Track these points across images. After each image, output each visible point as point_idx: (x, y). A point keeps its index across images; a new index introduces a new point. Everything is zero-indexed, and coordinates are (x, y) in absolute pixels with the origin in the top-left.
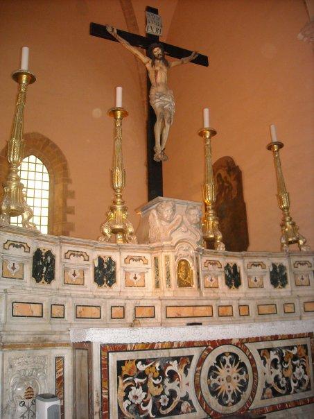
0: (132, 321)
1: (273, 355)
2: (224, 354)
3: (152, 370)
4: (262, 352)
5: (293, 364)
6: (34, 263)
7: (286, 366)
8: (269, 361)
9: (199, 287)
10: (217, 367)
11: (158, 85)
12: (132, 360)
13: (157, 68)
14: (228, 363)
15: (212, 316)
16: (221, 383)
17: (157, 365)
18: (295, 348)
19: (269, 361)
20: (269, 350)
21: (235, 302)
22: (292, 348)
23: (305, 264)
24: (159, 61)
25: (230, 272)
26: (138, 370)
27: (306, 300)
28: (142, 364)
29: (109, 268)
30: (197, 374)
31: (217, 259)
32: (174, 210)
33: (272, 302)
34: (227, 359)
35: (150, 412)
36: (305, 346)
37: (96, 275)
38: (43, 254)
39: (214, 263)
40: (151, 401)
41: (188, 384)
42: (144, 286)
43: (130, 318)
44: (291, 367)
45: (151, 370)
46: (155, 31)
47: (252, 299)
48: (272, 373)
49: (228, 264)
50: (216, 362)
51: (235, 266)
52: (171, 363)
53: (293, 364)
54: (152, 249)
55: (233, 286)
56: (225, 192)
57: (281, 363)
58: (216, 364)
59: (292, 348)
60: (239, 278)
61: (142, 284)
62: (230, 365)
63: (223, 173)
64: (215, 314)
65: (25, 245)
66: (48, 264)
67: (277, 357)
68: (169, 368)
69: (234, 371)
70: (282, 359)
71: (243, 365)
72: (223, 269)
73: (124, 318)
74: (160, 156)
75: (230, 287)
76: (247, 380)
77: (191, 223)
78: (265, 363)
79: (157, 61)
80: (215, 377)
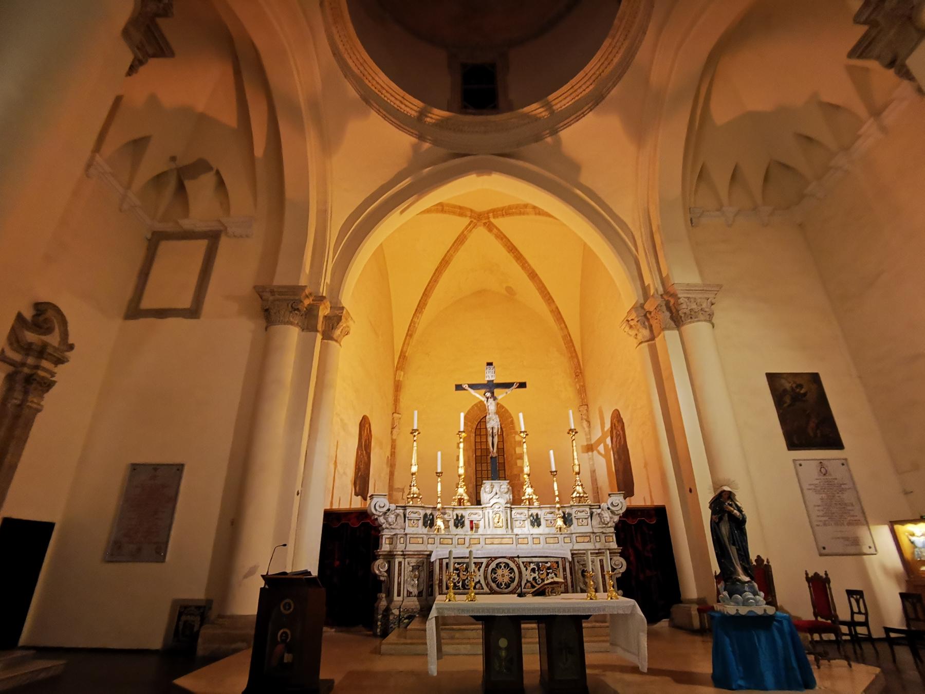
1: (532, 566)
2: (500, 563)
4: (525, 564)
5: (547, 572)
7: (542, 572)
8: (529, 569)
14: (503, 567)
16: (498, 577)
17: (465, 565)
19: (529, 569)
20: (530, 563)
22: (547, 563)
23: (416, 513)
27: (577, 535)
29: (461, 519)
30: (485, 571)
31: (523, 511)
33: (555, 536)
34: (503, 565)
35: (461, 586)
36: (557, 563)
37: (455, 523)
40: (461, 582)
41: (480, 576)
43: (467, 544)
44: (545, 574)
48: (531, 575)
51: (537, 515)
53: (547, 572)
55: (536, 526)
57: (538, 570)
59: (547, 563)
60: (540, 522)
63: (53, 339)
67: (535, 567)
69: (506, 572)
70: (539, 568)
71: (512, 569)
73: (464, 544)
76: (515, 577)
78: (527, 570)
80: (495, 573)
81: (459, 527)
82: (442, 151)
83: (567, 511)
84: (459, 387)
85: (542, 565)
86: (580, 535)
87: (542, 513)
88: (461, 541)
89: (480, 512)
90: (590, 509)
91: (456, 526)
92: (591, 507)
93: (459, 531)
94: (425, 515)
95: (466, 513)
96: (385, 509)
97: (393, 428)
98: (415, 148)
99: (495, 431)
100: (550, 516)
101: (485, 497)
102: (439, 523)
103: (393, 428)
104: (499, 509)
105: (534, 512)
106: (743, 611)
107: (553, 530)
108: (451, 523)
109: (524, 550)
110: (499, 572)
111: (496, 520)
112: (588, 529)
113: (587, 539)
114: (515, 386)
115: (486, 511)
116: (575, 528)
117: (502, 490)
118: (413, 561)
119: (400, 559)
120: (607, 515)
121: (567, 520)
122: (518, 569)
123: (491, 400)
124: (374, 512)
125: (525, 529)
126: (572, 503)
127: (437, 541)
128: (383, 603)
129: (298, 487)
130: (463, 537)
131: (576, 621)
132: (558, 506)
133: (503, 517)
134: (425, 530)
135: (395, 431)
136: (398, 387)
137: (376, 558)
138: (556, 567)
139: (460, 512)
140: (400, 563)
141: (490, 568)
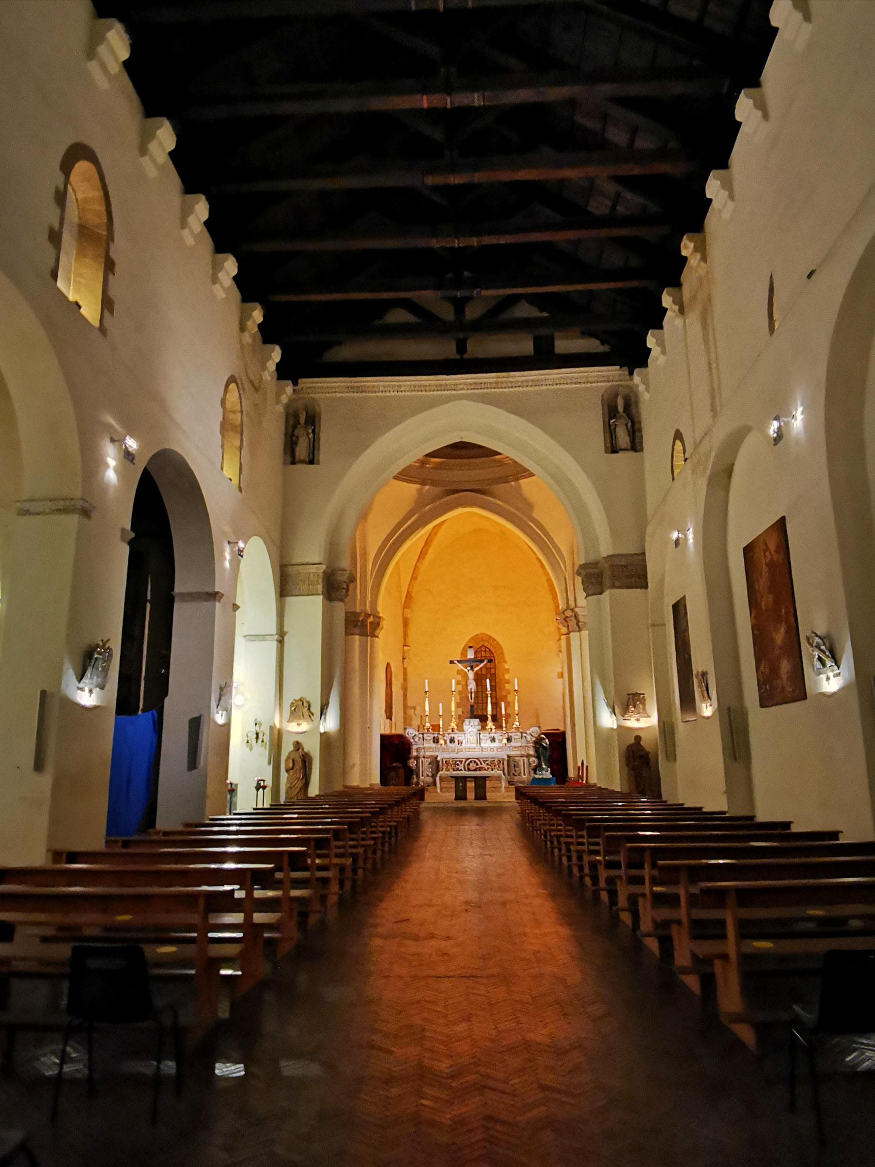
82: (437, 490)
83: (510, 734)
84: (452, 662)
87: (496, 736)
89: (463, 735)
91: (451, 742)
92: (522, 733)
93: (452, 745)
94: (434, 738)
95: (456, 736)
96: (413, 735)
97: (404, 659)
98: (419, 491)
99: (472, 691)
100: (501, 738)
101: (466, 727)
102: (442, 742)
103: (404, 659)
105: (492, 735)
106: (541, 777)
107: (501, 745)
108: (448, 741)
109: (486, 754)
110: (471, 765)
111: (471, 740)
112: (519, 744)
115: (466, 735)
116: (513, 744)
118: (429, 760)
119: (423, 759)
120: (529, 737)
121: (509, 740)
123: (471, 671)
124: (407, 736)
125: (486, 744)
126: (512, 730)
127: (441, 750)
128: (415, 780)
129: (368, 725)
131: (485, 778)
132: (504, 732)
133: (475, 738)
134: (434, 745)
135: (405, 661)
136: (406, 623)
137: (409, 758)
139: (452, 735)
140: (422, 762)
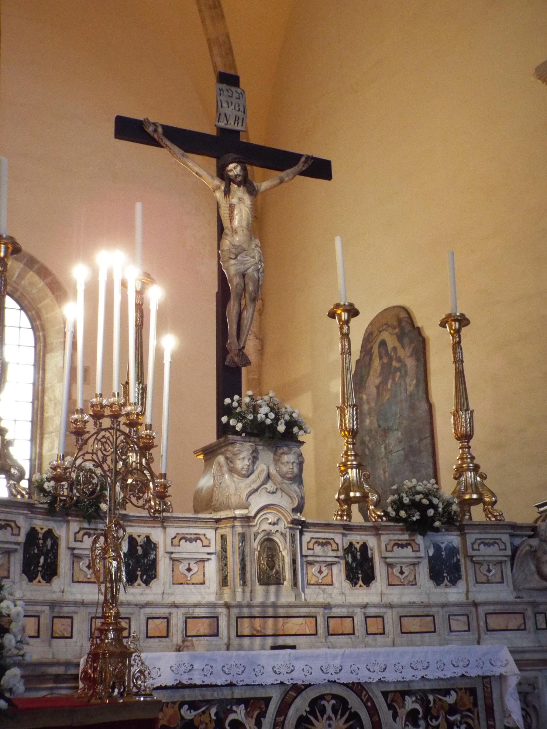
0: (180, 642)
1: (410, 703)
2: (322, 697)
3: (205, 718)
5: (447, 720)
6: (26, 552)
8: (402, 713)
9: (295, 584)
10: (311, 718)
11: (234, 231)
12: (174, 703)
13: (234, 201)
15: (316, 634)
17: (213, 711)
18: (452, 692)
19: (402, 713)
21: (358, 610)
23: (493, 544)
24: (236, 186)
25: (354, 557)
26: (182, 718)
27: (491, 608)
28: (189, 709)
29: (146, 554)
31: (330, 536)
32: (254, 459)
33: (426, 611)
34: (329, 705)
38: (41, 536)
39: (324, 543)
42: (203, 583)
43: (177, 637)
45: (203, 718)
46: (231, 121)
47: (391, 606)
49: (351, 544)
50: (308, 709)
51: (364, 546)
52: (234, 708)
53: (447, 720)
54: (218, 521)
55: (360, 582)
56: (394, 379)
57: (425, 718)
58: (310, 713)
60: (372, 568)
61: (199, 579)
62: (333, 716)
64: (321, 630)
65: (13, 524)
66: (48, 552)
67: (417, 706)
68: (232, 717)
71: (355, 716)
72: (341, 553)
74: (236, 359)
75: (354, 584)
77: (283, 477)
78: (395, 716)
79: (234, 187)
81: (139, 581)
85: (435, 701)
86: (498, 608)
88: (156, 626)
90: (512, 536)
94: (32, 534)
104: (276, 528)
113: (515, 622)
114: (300, 166)
117: (285, 469)
122: (371, 716)
130: (164, 611)
138: (470, 706)
141: (292, 715)
